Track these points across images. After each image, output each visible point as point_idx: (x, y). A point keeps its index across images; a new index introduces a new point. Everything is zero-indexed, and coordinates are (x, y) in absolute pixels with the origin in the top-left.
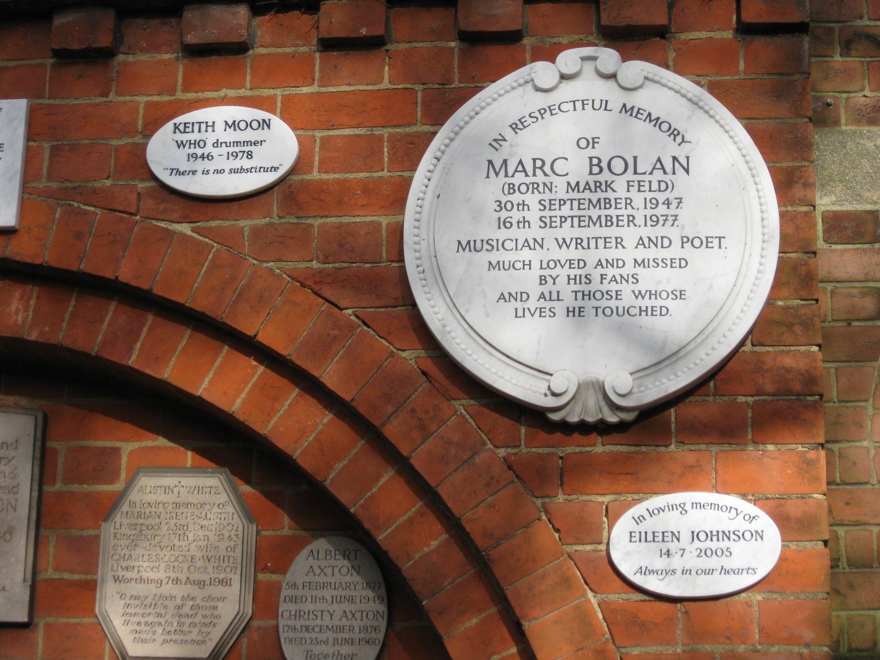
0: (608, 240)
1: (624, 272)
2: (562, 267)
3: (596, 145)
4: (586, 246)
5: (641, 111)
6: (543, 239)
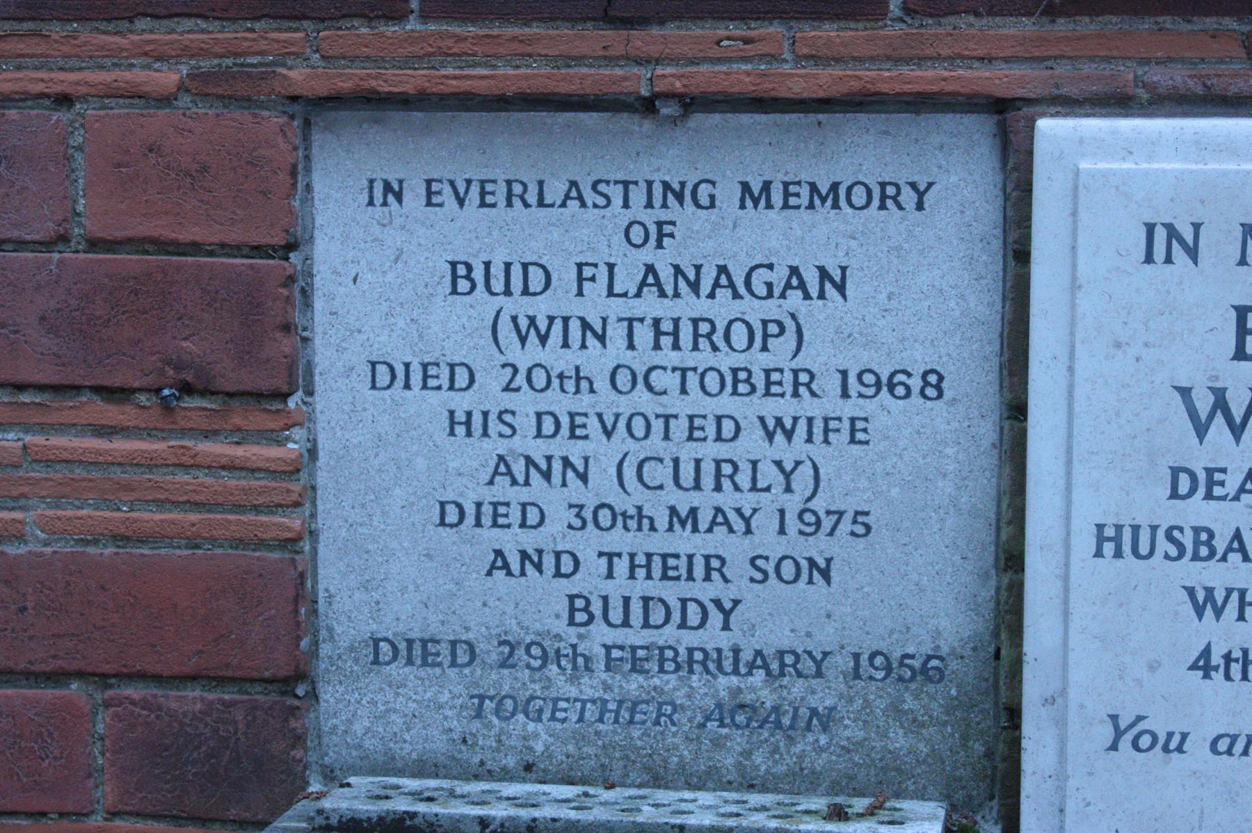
3: (666, 241)
5: (792, 189)
6: (1197, 227)
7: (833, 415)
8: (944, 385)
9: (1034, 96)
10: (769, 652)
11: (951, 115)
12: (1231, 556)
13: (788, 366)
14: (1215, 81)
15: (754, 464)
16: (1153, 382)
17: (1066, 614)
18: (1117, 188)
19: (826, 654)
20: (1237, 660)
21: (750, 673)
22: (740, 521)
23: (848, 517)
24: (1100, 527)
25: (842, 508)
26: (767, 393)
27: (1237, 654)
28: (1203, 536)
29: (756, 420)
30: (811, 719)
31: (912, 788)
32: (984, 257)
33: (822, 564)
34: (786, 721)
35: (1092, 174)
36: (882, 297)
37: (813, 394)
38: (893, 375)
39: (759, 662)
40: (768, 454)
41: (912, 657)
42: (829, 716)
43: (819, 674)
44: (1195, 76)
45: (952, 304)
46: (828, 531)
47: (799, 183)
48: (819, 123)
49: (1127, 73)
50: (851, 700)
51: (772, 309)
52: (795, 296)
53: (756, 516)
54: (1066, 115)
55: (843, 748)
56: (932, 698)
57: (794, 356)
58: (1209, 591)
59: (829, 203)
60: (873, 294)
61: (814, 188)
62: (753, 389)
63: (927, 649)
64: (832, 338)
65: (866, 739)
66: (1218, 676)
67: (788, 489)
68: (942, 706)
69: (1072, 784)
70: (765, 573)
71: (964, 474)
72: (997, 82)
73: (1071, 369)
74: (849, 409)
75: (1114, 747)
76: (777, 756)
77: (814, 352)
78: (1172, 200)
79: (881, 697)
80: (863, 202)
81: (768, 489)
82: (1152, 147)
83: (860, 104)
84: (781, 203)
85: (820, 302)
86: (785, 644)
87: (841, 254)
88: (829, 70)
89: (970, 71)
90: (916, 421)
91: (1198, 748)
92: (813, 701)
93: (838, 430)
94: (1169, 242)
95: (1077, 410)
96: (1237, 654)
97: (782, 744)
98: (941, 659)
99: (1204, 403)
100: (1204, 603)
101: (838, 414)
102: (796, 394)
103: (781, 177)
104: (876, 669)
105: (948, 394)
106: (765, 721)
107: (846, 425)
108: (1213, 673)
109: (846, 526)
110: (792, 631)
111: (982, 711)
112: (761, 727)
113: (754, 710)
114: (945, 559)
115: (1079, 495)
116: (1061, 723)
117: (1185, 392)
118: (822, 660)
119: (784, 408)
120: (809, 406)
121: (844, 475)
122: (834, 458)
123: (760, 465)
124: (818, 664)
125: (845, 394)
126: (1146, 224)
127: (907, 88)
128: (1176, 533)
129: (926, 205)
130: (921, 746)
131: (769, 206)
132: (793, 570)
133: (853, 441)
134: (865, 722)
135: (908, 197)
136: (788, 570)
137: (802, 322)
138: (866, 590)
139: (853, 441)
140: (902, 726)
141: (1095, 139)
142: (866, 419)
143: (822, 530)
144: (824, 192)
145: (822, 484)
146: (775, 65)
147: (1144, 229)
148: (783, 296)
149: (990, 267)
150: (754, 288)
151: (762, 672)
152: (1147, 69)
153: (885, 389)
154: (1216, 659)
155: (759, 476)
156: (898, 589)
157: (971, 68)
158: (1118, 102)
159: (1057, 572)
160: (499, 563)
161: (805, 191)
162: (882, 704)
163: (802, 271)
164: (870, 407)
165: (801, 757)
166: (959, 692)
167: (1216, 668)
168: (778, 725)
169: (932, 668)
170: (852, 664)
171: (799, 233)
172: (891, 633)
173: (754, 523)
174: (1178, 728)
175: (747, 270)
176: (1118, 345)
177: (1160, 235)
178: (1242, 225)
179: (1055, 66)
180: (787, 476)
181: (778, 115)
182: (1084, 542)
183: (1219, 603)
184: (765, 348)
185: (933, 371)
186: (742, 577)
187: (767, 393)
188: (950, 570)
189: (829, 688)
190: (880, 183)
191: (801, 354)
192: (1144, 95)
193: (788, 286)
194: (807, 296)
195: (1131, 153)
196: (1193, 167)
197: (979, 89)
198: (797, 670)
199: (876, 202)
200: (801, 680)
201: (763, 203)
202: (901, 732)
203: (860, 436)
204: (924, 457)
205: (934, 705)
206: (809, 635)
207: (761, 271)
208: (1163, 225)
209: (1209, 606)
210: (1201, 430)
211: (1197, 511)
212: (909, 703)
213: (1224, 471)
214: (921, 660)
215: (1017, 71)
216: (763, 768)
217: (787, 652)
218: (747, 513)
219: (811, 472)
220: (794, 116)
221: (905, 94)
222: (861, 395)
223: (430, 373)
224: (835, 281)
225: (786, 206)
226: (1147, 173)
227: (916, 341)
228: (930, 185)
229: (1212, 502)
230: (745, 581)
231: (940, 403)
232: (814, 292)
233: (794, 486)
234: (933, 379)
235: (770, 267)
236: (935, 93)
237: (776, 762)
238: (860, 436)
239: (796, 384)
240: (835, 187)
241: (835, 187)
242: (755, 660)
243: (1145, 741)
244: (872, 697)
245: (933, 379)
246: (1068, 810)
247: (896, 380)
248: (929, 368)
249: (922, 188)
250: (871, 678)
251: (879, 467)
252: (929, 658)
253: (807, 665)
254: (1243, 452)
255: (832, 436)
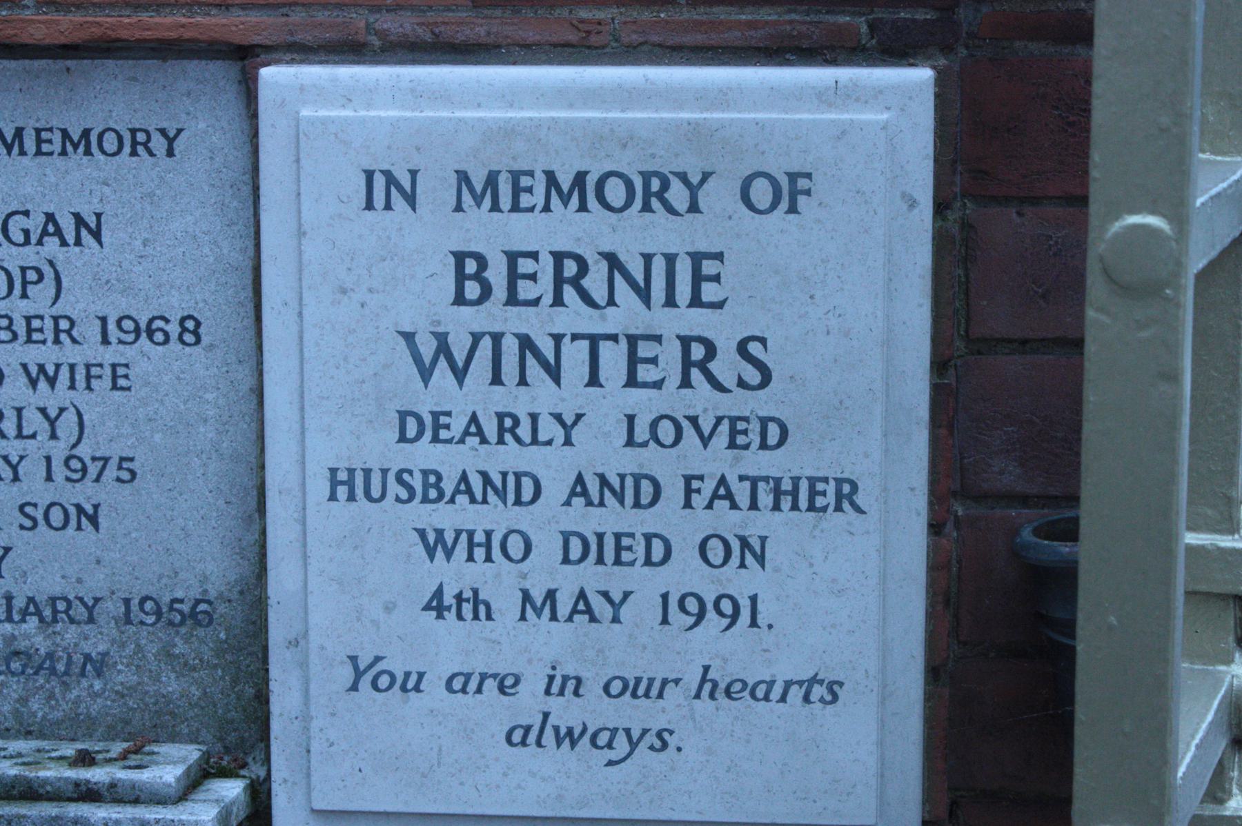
0: (644, 350)
1: (703, 521)
2: (705, 441)
4: (527, 438)
5: (44, 135)
6: (414, 173)
7: (94, 362)
8: (202, 330)
9: (270, 43)
10: (41, 598)
11: (196, 62)
12: (459, 498)
13: (47, 312)
14: (442, 29)
15: (19, 411)
16: (377, 328)
17: (305, 557)
18: (336, 135)
19: (97, 600)
20: (468, 600)
21: (23, 620)
22: (8, 468)
23: (113, 464)
24: (333, 471)
25: (107, 454)
26: (29, 340)
27: (468, 594)
28: (432, 478)
29: (19, 367)
30: (84, 665)
31: (186, 731)
32: (235, 203)
33: (90, 510)
34: (61, 667)
35: (312, 121)
36: (138, 243)
37: (74, 341)
38: (151, 321)
39: (32, 609)
40: (32, 401)
41: (181, 601)
42: (102, 661)
43: (91, 620)
44: (423, 24)
45: (206, 250)
46: (94, 477)
47: (50, 130)
48: (68, 69)
49: (358, 20)
50: (123, 645)
51: (30, 256)
52: (52, 243)
53: (23, 463)
54: (301, 62)
55: (117, 692)
56: (202, 641)
57: (54, 304)
58: (440, 533)
59: (81, 149)
60: (128, 240)
61: (65, 134)
62: (15, 337)
63: (195, 593)
64: (90, 284)
65: (139, 684)
66: (451, 616)
67: (54, 436)
68: (212, 649)
69: (315, 725)
70: (34, 520)
71: (225, 418)
72: (234, 28)
73: (300, 314)
74: (109, 355)
75: (354, 687)
76: (53, 702)
77: (72, 299)
78: (389, 147)
79: (152, 641)
80: (114, 148)
81: (33, 436)
82: (370, 95)
83: (108, 50)
84: (34, 149)
85: (77, 249)
86: (57, 591)
87: (95, 201)
88: (70, 17)
89: (208, 18)
90: (176, 366)
91: (434, 686)
92: (86, 647)
93: (100, 377)
94: (388, 188)
95: (306, 355)
96: (468, 594)
97: (57, 690)
98: (209, 602)
99: (427, 348)
100: (435, 544)
101: (99, 360)
102: (57, 341)
103: (32, 123)
104: (147, 614)
105: (205, 340)
106: (40, 667)
107: (108, 371)
108: (446, 613)
109: (111, 472)
110: (63, 577)
111: (250, 654)
112: (36, 673)
113: (29, 656)
114: (209, 504)
115: (313, 439)
116: (304, 665)
117: (409, 337)
118: (94, 606)
119: (46, 354)
120: (71, 353)
121: (108, 422)
122: (98, 404)
123: (24, 412)
124: (90, 610)
125: (105, 341)
126: (365, 171)
127: (147, 34)
128: (406, 476)
129: (176, 152)
130: (193, 689)
131: (22, 153)
132: (62, 517)
133: (115, 387)
134: (138, 667)
135: (158, 143)
136: (56, 516)
137: (59, 269)
138: (133, 535)
139: (115, 387)
140: (173, 670)
141: (314, 85)
142: (127, 366)
143: (88, 476)
144: (76, 138)
145: (86, 431)
146: (17, 11)
147: (363, 176)
148: (40, 242)
149: (241, 213)
150: (11, 235)
151: (35, 619)
152: (378, 16)
153: (144, 335)
154: (448, 600)
155: (24, 424)
156: (165, 535)
157: (209, 15)
158: (351, 49)
159: (296, 515)
160: (722, 491)
161: (57, 137)
162: (153, 649)
163: (57, 217)
164: (129, 353)
165: (77, 702)
166: (227, 635)
167: (449, 608)
168: (53, 671)
169: (201, 612)
170: (123, 609)
171: (53, 179)
172: (160, 577)
173: (21, 471)
174: (414, 668)
175: (3, 216)
176: (344, 291)
177: (379, 182)
178: (457, 172)
179: (290, 13)
180: (52, 423)
181: (27, 62)
182: (319, 487)
183: (450, 544)
184: (24, 295)
185: (190, 317)
186: (11, 524)
187: (29, 340)
188: (215, 514)
189: (101, 633)
190: (130, 130)
191: (60, 300)
192: (376, 42)
193: (45, 233)
194: (64, 243)
195: (350, 100)
196: (408, 114)
197: (217, 36)
198: (69, 616)
199: (127, 149)
200: (74, 627)
201: (16, 150)
202: (173, 676)
203: (122, 382)
204: (185, 403)
205: (204, 649)
206: (79, 581)
207: (17, 217)
208: (381, 171)
209: (439, 548)
210: (426, 374)
211: (424, 454)
212: (180, 648)
213: (449, 414)
214: (190, 604)
215: (253, 17)
216: (40, 714)
217: (59, 598)
218: (15, 460)
219: (76, 419)
220: (43, 62)
221: (145, 40)
222: (121, 342)
223: (521, 270)
224: (90, 228)
225: (39, 152)
226: (363, 121)
227: (172, 287)
228: (179, 131)
229: (438, 445)
230: (15, 527)
231: (197, 349)
232: (70, 238)
233: (59, 433)
234: (190, 324)
235: (26, 213)
236: (175, 40)
237: (52, 708)
238: (122, 382)
239: (57, 331)
240: (86, 133)
241: (86, 133)
242: (27, 607)
243: (384, 681)
244: (144, 642)
245: (190, 324)
246: (312, 749)
247: (154, 326)
248: (186, 314)
249: (171, 135)
250: (142, 623)
251: (141, 413)
252: (198, 602)
253: (79, 611)
254: (466, 395)
255: (94, 383)
